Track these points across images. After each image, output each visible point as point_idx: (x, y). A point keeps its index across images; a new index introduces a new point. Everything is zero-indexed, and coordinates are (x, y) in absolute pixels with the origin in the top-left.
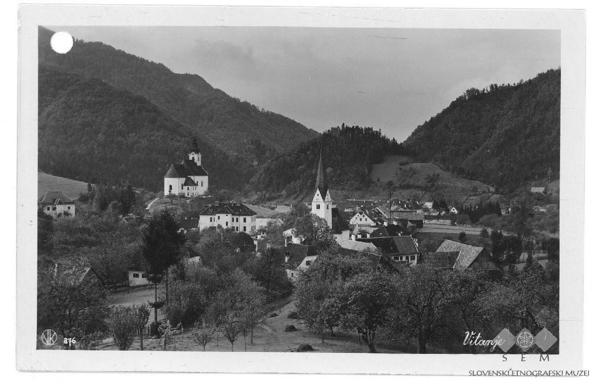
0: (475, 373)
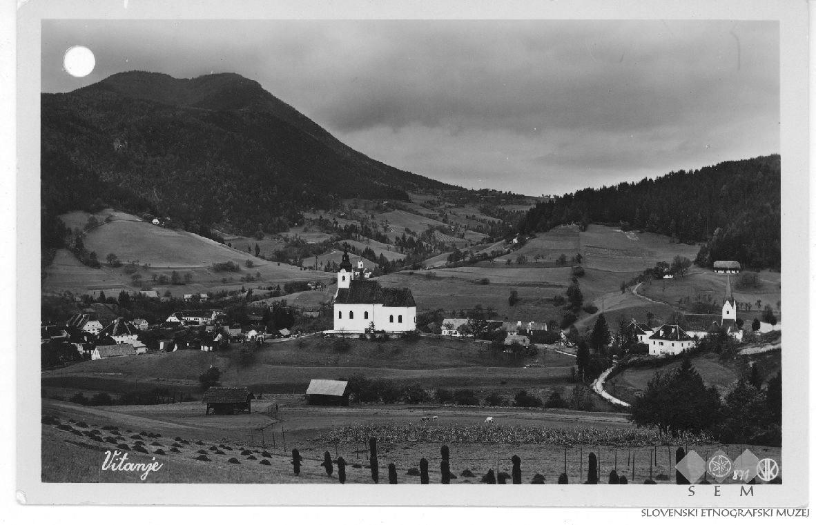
0: (650, 513)
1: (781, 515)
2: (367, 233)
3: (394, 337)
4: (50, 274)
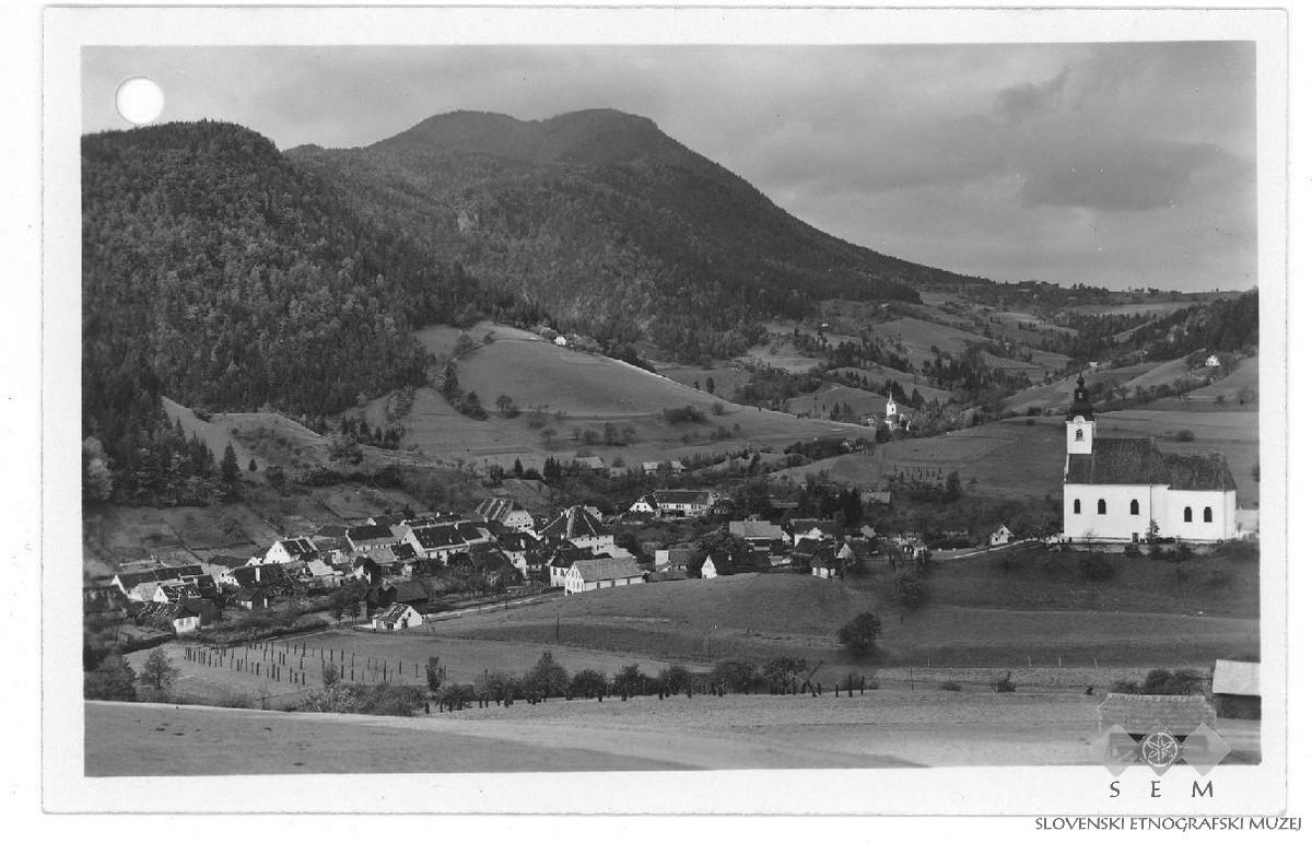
0: (1049, 824)
1: (1257, 827)
2: (874, 355)
3: (1200, 551)
4: (410, 430)
